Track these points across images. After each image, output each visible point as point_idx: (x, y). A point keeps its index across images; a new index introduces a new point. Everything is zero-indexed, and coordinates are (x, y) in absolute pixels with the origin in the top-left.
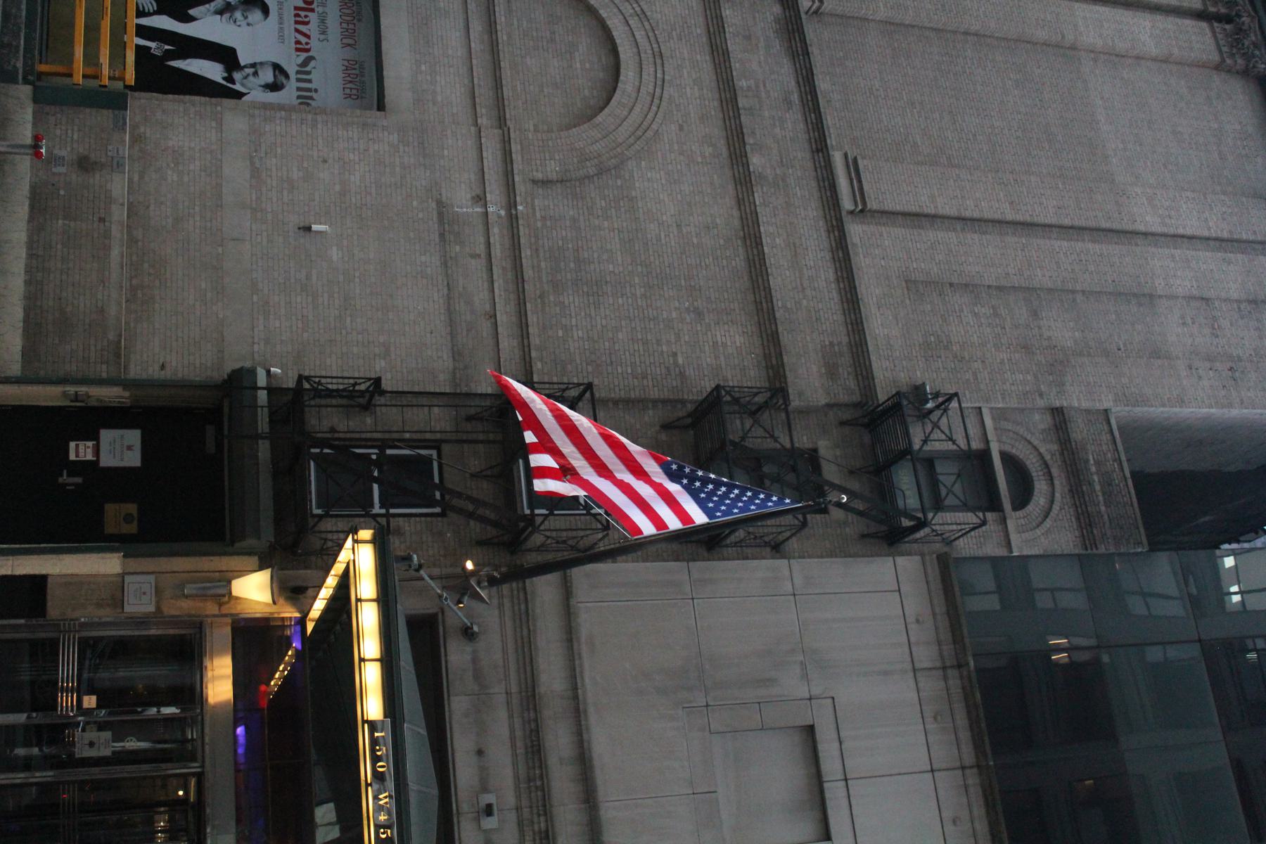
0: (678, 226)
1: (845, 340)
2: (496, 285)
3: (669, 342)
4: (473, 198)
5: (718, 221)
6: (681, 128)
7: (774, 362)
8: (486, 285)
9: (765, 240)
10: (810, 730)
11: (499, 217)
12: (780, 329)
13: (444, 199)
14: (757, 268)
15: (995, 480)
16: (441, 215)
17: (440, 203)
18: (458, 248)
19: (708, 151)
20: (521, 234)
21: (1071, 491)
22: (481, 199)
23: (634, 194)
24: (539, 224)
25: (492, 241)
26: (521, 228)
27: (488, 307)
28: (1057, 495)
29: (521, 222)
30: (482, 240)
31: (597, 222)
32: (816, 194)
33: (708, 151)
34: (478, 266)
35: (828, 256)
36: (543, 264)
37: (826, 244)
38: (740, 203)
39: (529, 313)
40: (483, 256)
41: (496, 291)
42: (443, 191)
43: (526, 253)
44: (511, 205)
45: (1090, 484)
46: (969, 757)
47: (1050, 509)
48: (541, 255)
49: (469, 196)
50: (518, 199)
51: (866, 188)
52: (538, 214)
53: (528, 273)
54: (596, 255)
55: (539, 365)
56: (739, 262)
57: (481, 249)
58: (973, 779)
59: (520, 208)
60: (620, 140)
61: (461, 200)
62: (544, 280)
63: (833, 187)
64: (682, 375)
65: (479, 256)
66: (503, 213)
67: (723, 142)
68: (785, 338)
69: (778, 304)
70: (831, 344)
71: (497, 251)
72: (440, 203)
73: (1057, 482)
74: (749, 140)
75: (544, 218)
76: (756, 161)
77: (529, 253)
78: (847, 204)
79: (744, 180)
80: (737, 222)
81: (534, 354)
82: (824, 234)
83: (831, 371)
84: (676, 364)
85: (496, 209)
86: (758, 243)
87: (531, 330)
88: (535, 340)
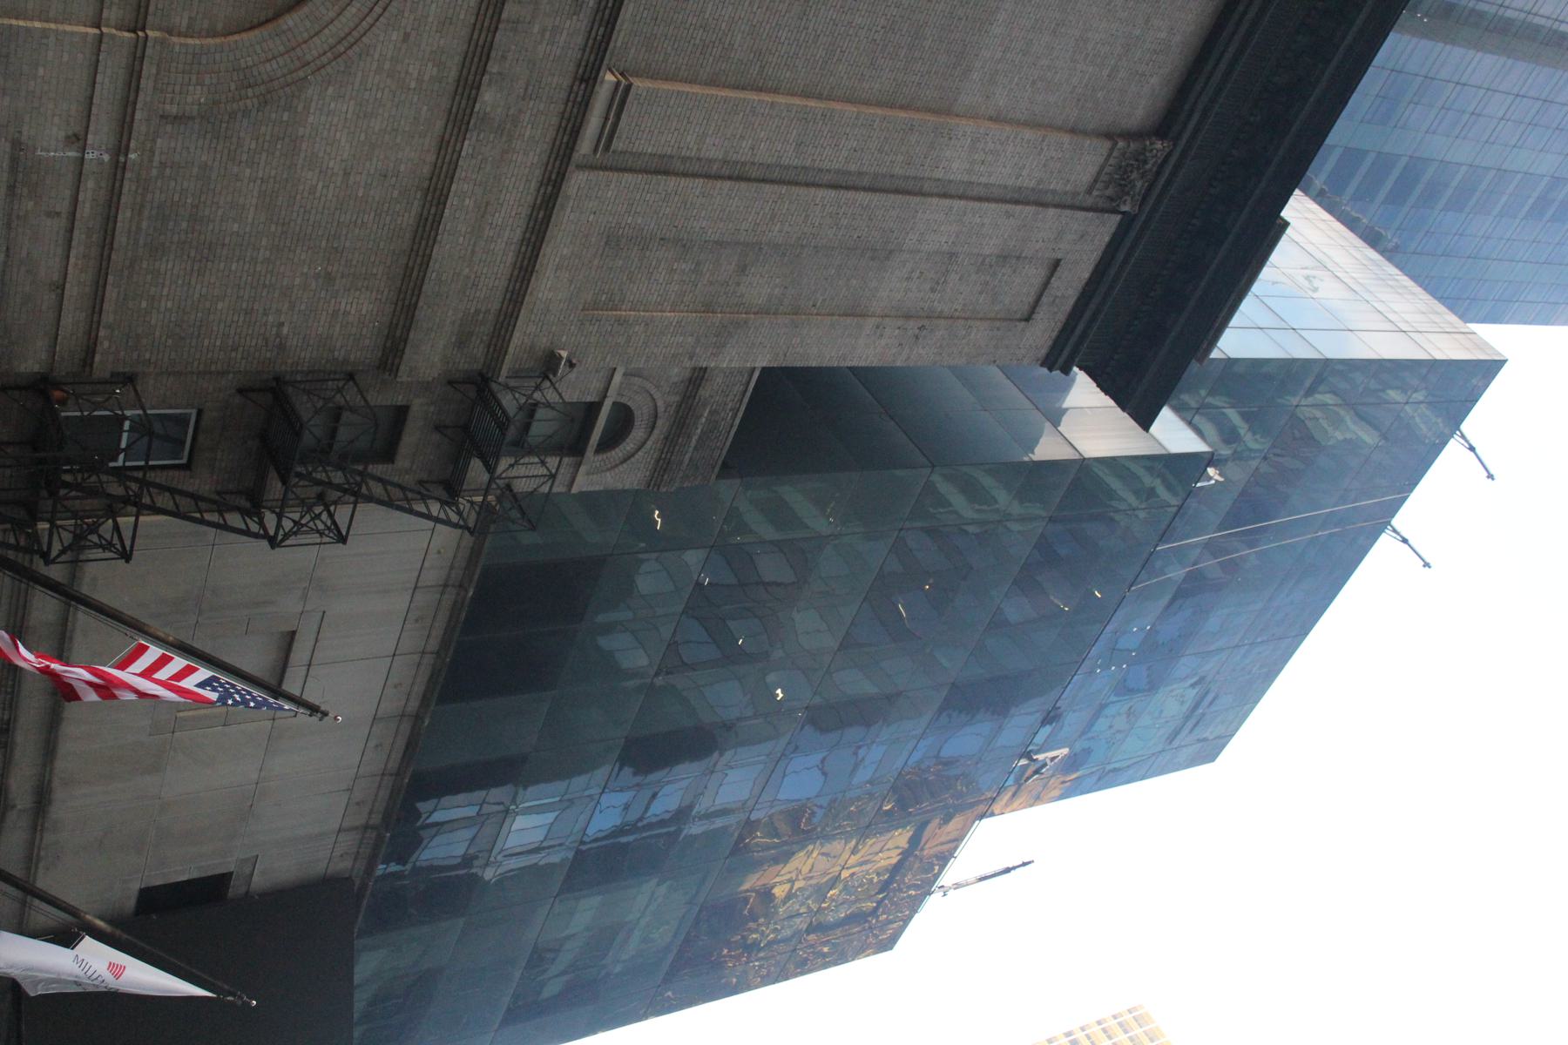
0: (346, 174)
1: (496, 306)
2: (73, 253)
3: (279, 311)
4: (68, 137)
5: (402, 168)
6: (406, 36)
7: (398, 333)
8: (59, 251)
9: (452, 200)
10: (292, 635)
11: (101, 162)
12: (421, 304)
13: (24, 139)
14: (428, 228)
15: (596, 418)
16: (14, 161)
17: (17, 144)
18: (31, 204)
19: (431, 71)
20: (125, 190)
21: (666, 438)
22: (78, 140)
23: (301, 131)
24: (154, 172)
25: (81, 198)
26: (126, 183)
27: (56, 277)
28: (649, 443)
29: (128, 175)
30: (68, 193)
31: (236, 169)
32: (551, 134)
33: (431, 71)
34: (52, 228)
35: (525, 211)
36: (144, 224)
37: (530, 199)
38: (442, 144)
39: (109, 287)
40: (64, 216)
41: (72, 260)
42: (25, 129)
43: (124, 215)
44: (120, 149)
45: (690, 437)
46: (434, 644)
47: (644, 443)
48: (146, 213)
49: (62, 134)
50: (132, 145)
51: (622, 124)
52: (157, 158)
53: (121, 239)
54: (220, 213)
55: (106, 344)
56: (408, 219)
57: (63, 207)
58: (429, 660)
59: (132, 156)
60: (308, 58)
61: (50, 142)
62: (141, 242)
63: (585, 105)
64: (281, 347)
65: (58, 214)
66: (106, 157)
67: (458, 59)
68: (421, 314)
69: (432, 275)
70: (477, 312)
71: (85, 210)
72: (17, 144)
73: (656, 432)
74: (493, 68)
75: (163, 165)
76: (489, 97)
77: (128, 214)
78: (585, 146)
79: (461, 116)
80: (426, 170)
81: (102, 333)
82: (534, 185)
83: (462, 341)
84: (278, 335)
85: (97, 154)
86: (441, 202)
87: (105, 306)
88: (108, 317)
